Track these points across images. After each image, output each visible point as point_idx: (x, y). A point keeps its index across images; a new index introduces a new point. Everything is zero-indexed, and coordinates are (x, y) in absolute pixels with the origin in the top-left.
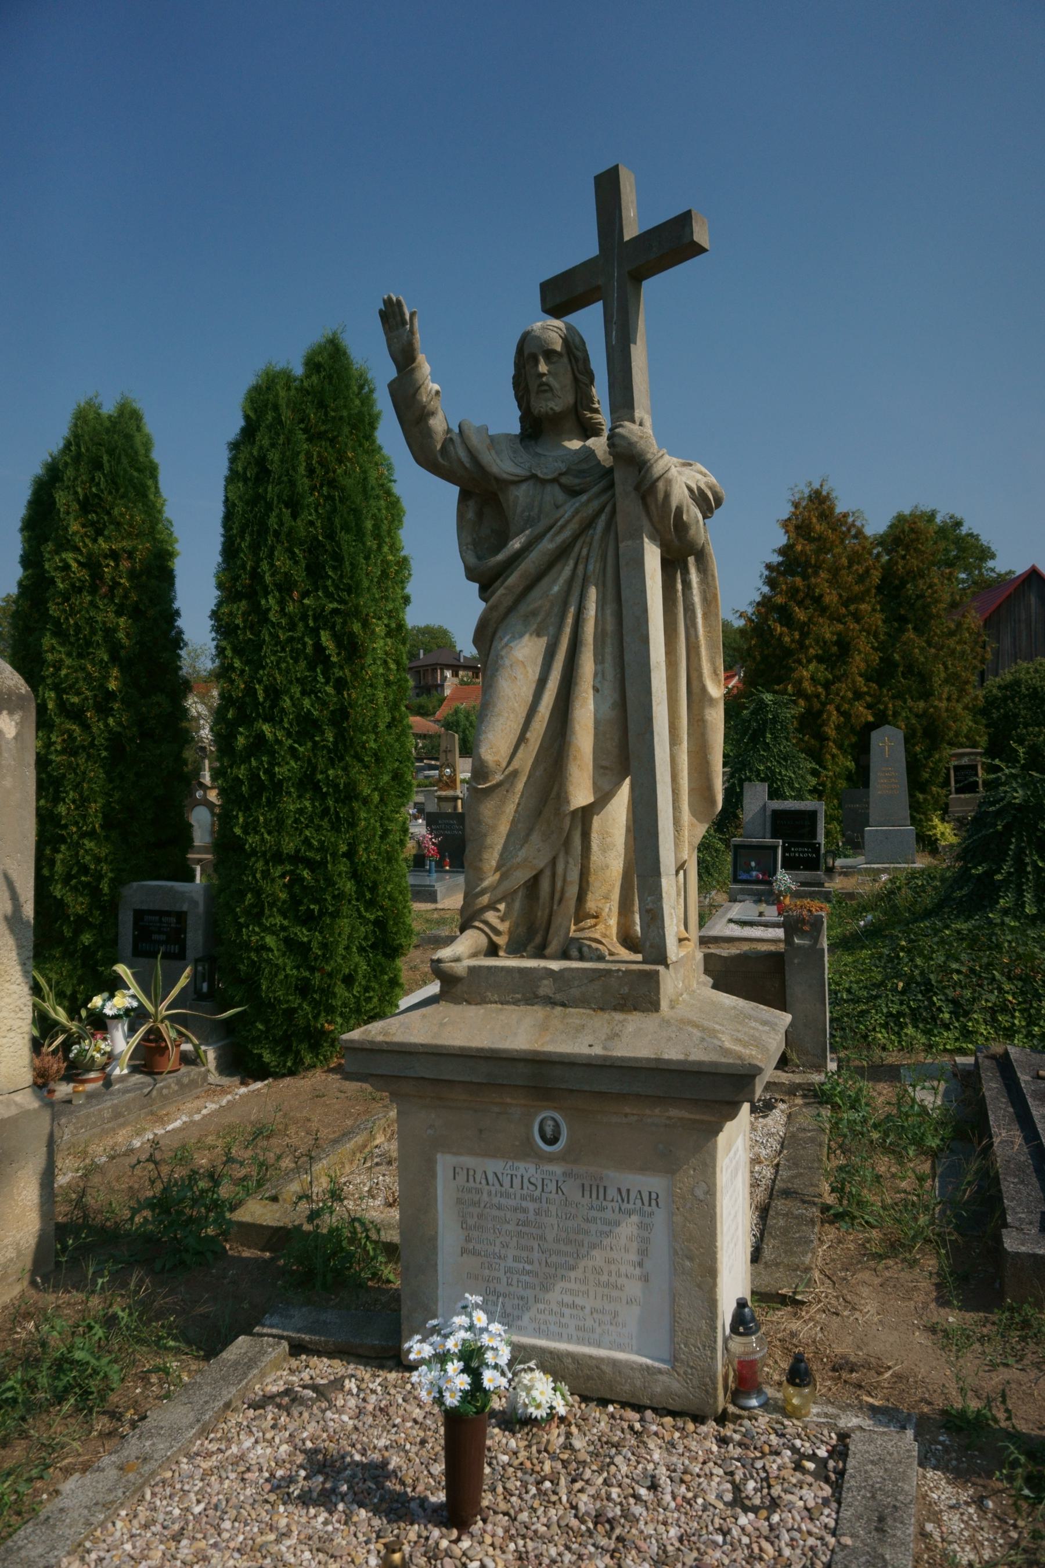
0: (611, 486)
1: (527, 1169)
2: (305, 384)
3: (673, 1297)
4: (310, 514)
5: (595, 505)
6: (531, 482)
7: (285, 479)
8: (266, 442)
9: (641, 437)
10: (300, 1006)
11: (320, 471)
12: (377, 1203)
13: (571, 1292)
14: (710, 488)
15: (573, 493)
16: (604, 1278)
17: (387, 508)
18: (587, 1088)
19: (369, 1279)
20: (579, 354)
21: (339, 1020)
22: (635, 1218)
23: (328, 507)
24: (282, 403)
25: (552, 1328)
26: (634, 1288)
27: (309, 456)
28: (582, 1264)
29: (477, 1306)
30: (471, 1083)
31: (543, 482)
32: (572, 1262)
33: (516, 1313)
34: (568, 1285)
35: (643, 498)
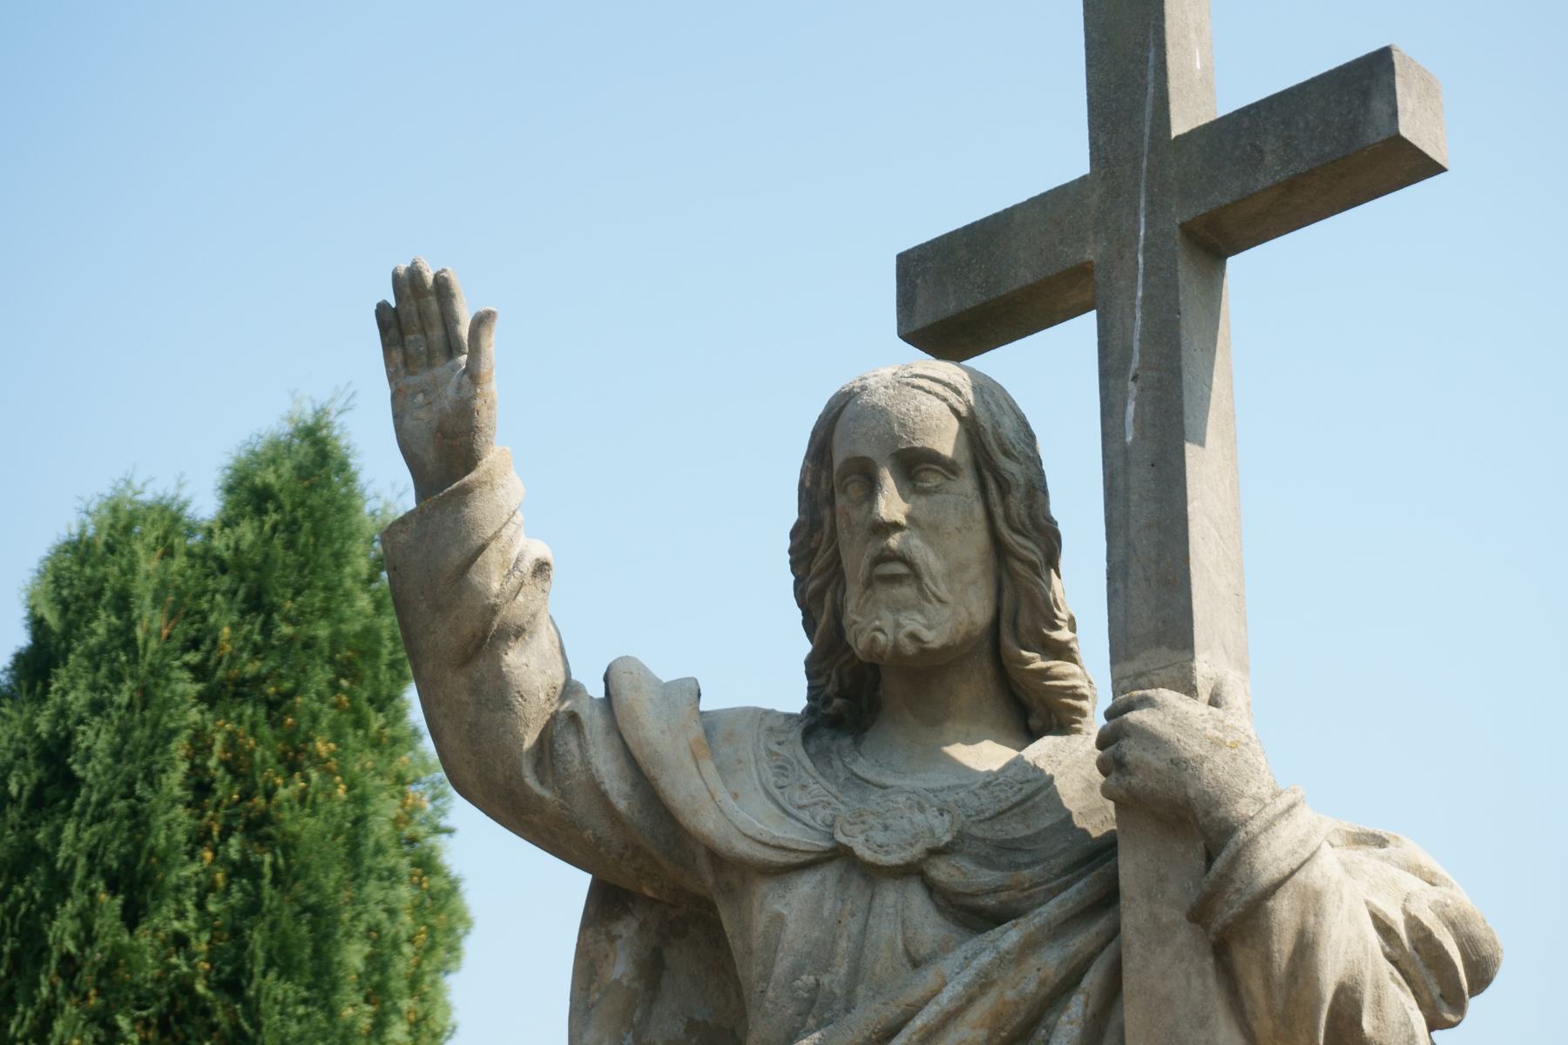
0: (1108, 898)
2: (218, 543)
4: (181, 915)
5: (1050, 962)
6: (830, 874)
7: (119, 805)
8: (79, 699)
9: (1217, 744)
11: (225, 789)
14: (1453, 925)
15: (972, 916)
17: (418, 908)
20: (1009, 467)
23: (236, 897)
24: (143, 589)
27: (200, 743)
31: (872, 874)
35: (1221, 951)
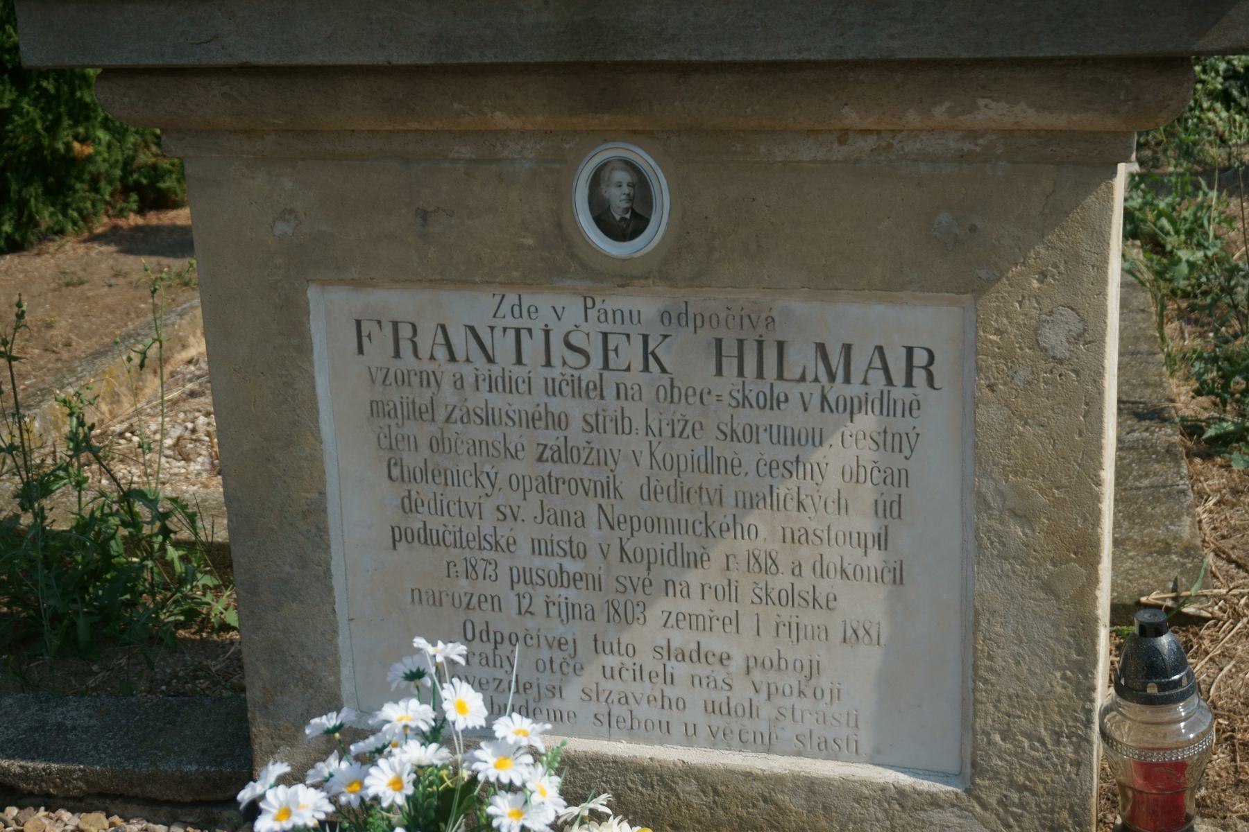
1: (560, 310)
3: (973, 620)
10: (15, 108)
12: (194, 467)
13: (692, 621)
16: (782, 581)
18: (734, 53)
19: (178, 625)
21: (102, 135)
22: (867, 422)
25: (643, 711)
26: (865, 603)
28: (718, 551)
29: (449, 671)
30: (389, 71)
32: (690, 544)
33: (546, 680)
34: (684, 606)
